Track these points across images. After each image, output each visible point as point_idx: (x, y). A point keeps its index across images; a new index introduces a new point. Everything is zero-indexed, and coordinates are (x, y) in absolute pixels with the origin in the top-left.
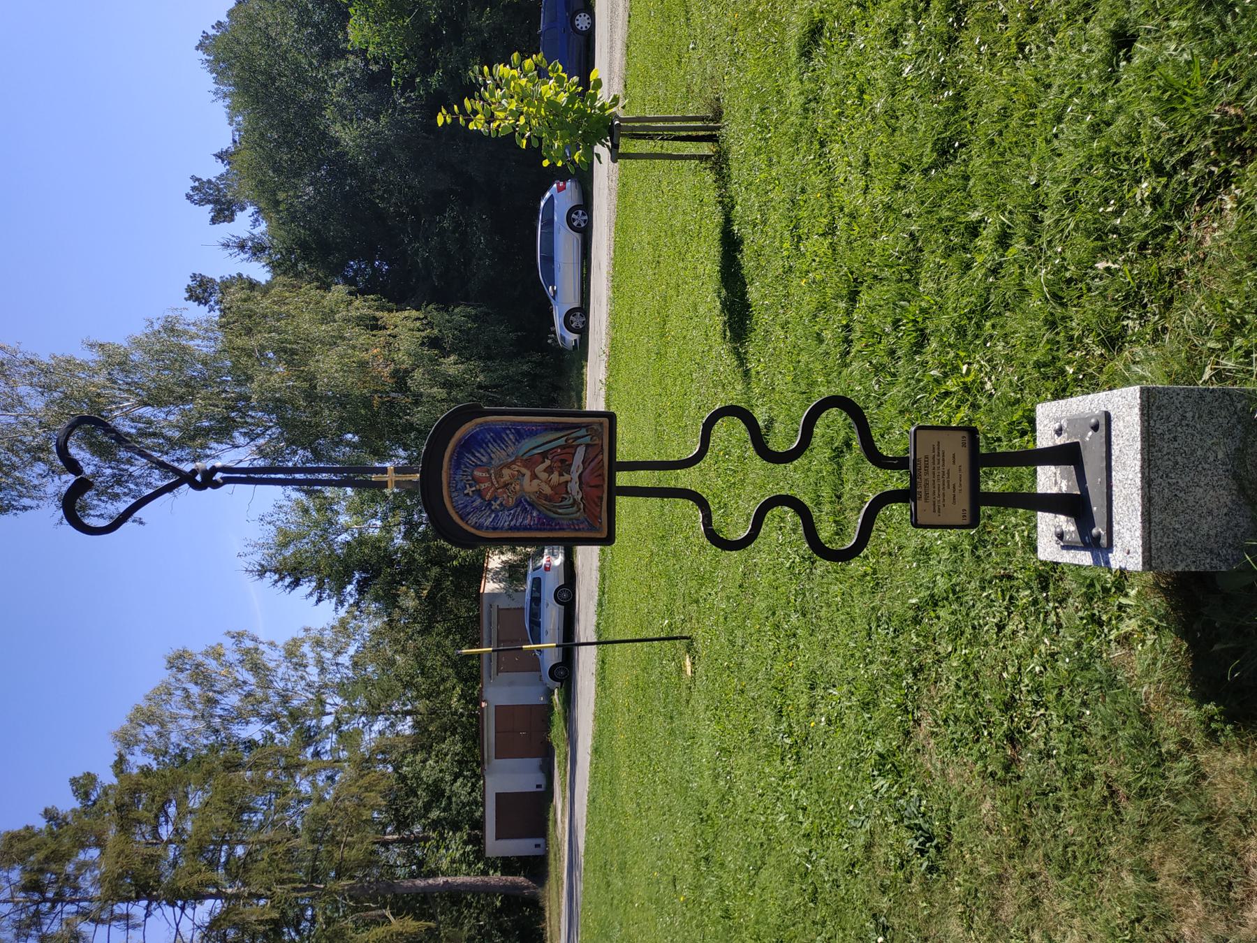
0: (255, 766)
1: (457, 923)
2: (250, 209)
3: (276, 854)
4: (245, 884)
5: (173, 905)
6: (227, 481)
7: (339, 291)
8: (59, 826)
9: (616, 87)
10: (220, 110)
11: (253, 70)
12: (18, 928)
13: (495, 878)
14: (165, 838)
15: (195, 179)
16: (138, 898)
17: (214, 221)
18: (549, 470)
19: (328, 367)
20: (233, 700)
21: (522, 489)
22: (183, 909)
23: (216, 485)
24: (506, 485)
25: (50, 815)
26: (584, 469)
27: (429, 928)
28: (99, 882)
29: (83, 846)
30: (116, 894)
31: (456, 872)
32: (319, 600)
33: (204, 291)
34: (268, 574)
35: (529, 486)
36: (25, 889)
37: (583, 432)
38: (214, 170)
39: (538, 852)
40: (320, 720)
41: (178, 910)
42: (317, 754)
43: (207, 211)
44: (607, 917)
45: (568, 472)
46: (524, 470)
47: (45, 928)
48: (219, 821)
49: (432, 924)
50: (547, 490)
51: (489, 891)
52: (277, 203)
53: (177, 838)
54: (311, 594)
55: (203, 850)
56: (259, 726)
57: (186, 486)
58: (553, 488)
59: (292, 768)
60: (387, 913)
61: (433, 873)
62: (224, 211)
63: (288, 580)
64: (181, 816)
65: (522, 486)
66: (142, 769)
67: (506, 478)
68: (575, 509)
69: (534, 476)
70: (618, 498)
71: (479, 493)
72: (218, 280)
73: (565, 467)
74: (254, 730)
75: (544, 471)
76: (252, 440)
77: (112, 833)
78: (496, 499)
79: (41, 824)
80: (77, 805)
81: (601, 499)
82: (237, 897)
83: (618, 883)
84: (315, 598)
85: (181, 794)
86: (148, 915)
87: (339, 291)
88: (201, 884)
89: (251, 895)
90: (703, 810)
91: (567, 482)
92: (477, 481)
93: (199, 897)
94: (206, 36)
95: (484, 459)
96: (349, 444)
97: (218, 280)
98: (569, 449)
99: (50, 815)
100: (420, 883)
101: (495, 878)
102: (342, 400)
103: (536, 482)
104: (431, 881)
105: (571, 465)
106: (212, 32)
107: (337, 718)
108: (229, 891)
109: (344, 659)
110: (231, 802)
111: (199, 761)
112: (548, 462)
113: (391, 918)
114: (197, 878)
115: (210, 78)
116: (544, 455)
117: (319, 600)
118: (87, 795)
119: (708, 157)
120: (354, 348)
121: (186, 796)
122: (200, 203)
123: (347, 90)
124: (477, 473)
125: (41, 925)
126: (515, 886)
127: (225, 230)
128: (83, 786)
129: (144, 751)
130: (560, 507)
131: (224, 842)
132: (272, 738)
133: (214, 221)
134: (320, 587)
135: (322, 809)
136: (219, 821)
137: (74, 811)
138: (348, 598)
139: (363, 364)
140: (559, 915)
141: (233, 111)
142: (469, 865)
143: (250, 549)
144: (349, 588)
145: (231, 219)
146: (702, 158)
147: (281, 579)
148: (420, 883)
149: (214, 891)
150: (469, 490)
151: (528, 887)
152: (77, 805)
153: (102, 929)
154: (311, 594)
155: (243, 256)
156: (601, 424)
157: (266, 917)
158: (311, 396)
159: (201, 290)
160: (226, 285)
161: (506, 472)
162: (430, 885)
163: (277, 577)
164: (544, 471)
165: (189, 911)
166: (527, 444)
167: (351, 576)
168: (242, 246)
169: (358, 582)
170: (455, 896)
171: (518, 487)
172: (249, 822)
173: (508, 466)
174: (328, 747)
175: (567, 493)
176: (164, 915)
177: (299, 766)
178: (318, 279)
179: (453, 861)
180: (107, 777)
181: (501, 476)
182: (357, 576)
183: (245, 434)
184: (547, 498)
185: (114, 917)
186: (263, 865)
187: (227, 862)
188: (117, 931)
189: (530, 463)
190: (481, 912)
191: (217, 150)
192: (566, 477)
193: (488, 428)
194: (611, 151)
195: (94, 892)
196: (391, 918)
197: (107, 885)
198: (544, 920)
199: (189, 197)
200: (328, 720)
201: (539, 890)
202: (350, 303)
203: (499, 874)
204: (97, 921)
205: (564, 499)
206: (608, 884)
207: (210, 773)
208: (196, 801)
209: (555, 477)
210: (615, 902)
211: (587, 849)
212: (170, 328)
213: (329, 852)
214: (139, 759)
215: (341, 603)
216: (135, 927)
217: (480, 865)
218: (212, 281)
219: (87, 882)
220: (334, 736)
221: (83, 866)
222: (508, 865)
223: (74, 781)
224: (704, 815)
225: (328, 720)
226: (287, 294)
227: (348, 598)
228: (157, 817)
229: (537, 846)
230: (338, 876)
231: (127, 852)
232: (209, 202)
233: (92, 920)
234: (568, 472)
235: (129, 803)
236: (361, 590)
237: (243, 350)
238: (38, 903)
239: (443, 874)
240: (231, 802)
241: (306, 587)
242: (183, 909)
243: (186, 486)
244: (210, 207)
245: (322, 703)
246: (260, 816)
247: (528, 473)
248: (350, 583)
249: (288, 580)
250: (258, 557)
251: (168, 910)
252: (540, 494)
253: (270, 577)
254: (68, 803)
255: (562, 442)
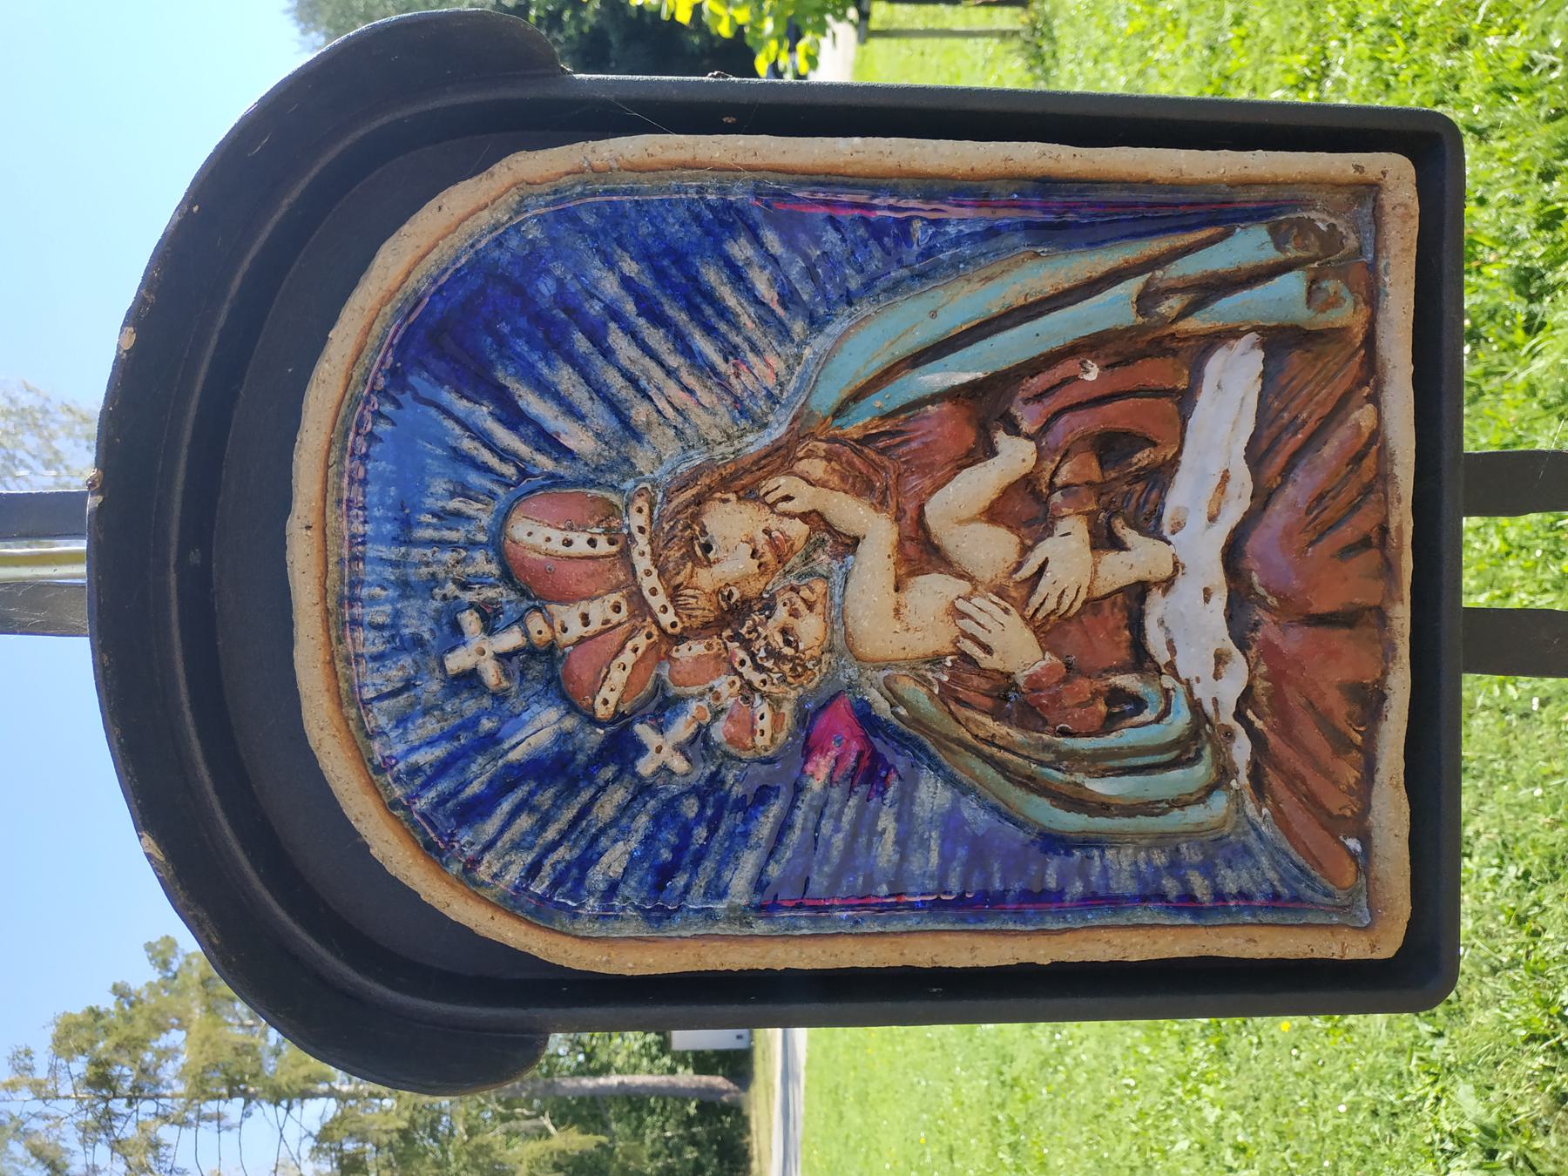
1: (637, 1134)
5: (277, 1104)
9: (751, 310)
12: (85, 1131)
13: (686, 1078)
16: (231, 1095)
18: (1024, 509)
21: (841, 643)
24: (733, 614)
25: (120, 991)
26: (1263, 498)
27: (600, 1145)
28: (180, 1076)
29: (162, 1029)
31: (635, 1069)
35: (892, 621)
36: (89, 1083)
37: (1248, 246)
39: (741, 1045)
41: (281, 1111)
44: (839, 1160)
45: (1150, 524)
46: (850, 512)
47: (117, 1132)
49: (604, 1139)
50: (1016, 650)
51: (682, 1096)
58: (1047, 630)
60: (546, 1121)
61: (605, 1069)
65: (837, 618)
67: (733, 566)
68: (1201, 772)
69: (922, 552)
70: (1468, 680)
71: (543, 667)
73: (1127, 482)
75: (994, 514)
77: (197, 1012)
78: (663, 706)
79: (108, 1003)
80: (155, 976)
81: (1370, 701)
82: (354, 1096)
83: (854, 1117)
86: (247, 1115)
88: (308, 1079)
90: (1005, 1068)
91: (1139, 592)
92: (530, 586)
95: (578, 439)
98: (1157, 362)
99: (120, 991)
100: (588, 1083)
101: (686, 1078)
103: (933, 590)
104: (602, 1081)
105: (1162, 475)
112: (1016, 454)
113: (552, 1129)
116: (987, 407)
118: (165, 965)
119: (1015, 33)
124: (537, 535)
125: (111, 1128)
126: (711, 1090)
130: (1101, 764)
137: (150, 985)
140: (770, 1130)
142: (652, 1060)
146: (1004, 35)
148: (588, 1083)
150: (478, 652)
151: (728, 1091)
152: (155, 976)
153: (187, 1134)
156: (1368, 191)
161: (732, 525)
162: (602, 1087)
164: (994, 514)
165: (296, 1111)
166: (869, 339)
170: (635, 1102)
171: (810, 629)
173: (743, 482)
175: (1140, 659)
176: (265, 1113)
179: (631, 1054)
181: (701, 551)
184: (1006, 696)
185: (201, 1117)
188: (207, 1131)
189: (886, 457)
190: (667, 1119)
192: (1141, 557)
193: (607, 220)
194: (857, 26)
195: (180, 1088)
196: (552, 1129)
197: (190, 1080)
198: (749, 1132)
201: (743, 1095)
203: (690, 1071)
204: (184, 1124)
205: (1123, 706)
206: (841, 1116)
209: (1068, 561)
210: (852, 1143)
211: (809, 1061)
216: (229, 1128)
217: (667, 1060)
219: (168, 1071)
221: (167, 1053)
222: (703, 1062)
223: (149, 947)
224: (1008, 1078)
229: (739, 1037)
231: (214, 1040)
234: (1150, 524)
238: (106, 1100)
239: (618, 1071)
242: (288, 1109)
247: (878, 532)
251: (269, 1109)
252: (962, 676)
254: (108, 1003)
255: (1113, 309)
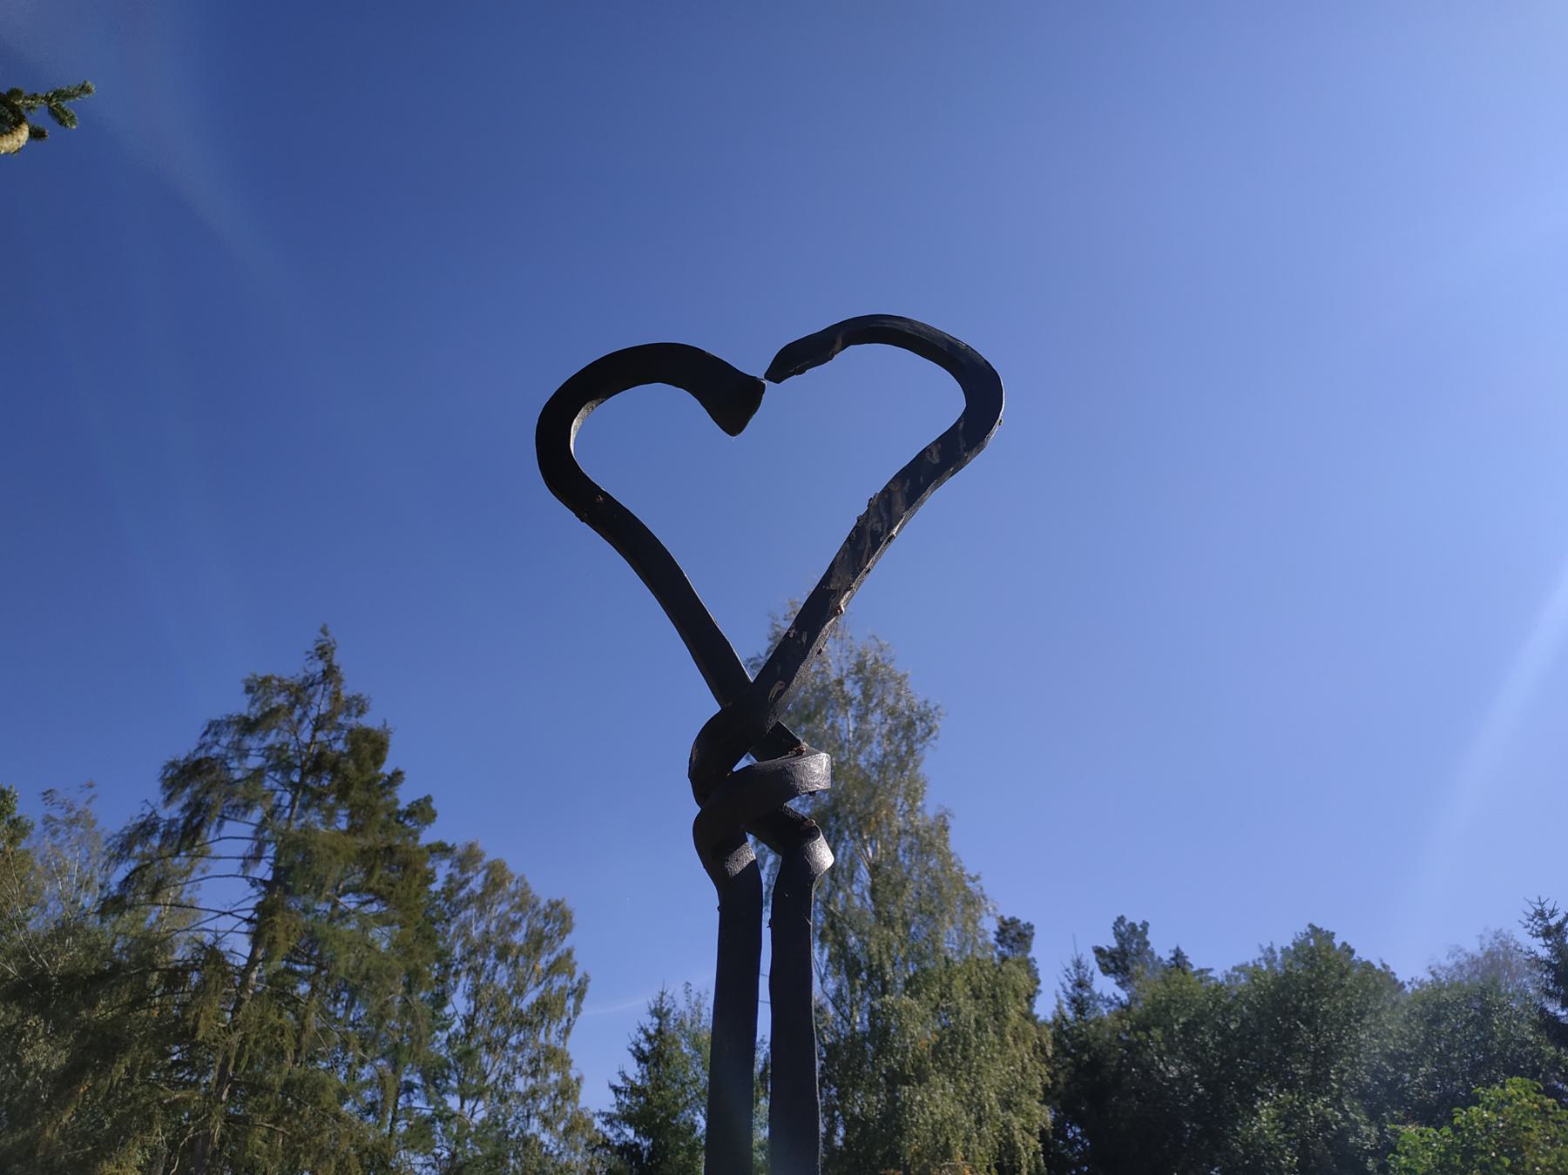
0: (407, 1009)
2: (1123, 996)
3: (282, 1034)
4: (257, 995)
5: (256, 910)
6: (737, 902)
7: (1045, 1116)
8: (381, 787)
10: (1250, 955)
11: (1313, 994)
14: (341, 900)
15: (1145, 925)
17: (1099, 951)
19: (937, 1102)
20: (502, 976)
22: (249, 921)
23: (713, 843)
25: (396, 777)
30: (289, 844)
32: (616, 1090)
33: (1014, 939)
34: (656, 1021)
38: (1161, 947)
40: (454, 1092)
41: (247, 915)
42: (409, 1087)
43: (1110, 942)
48: (346, 962)
52: (1146, 1029)
53: (336, 914)
54: (625, 1078)
55: (312, 947)
56: (462, 1011)
57: (711, 707)
59: (395, 1055)
62: (1117, 961)
63: (646, 1047)
64: (363, 919)
66: (432, 871)
72: (1030, 956)
74: (459, 1004)
76: (834, 1002)
84: (620, 1083)
85: (392, 917)
87: (1045, 1116)
88: (273, 940)
89: (240, 1001)
93: (256, 939)
94: (1331, 936)
96: (831, 1131)
97: (1030, 956)
102: (894, 1120)
106: (1338, 942)
107: (454, 1115)
108: (254, 975)
109: (535, 1125)
110: (367, 977)
111: (430, 939)
114: (281, 936)
115: (1288, 943)
117: (616, 1090)
120: (968, 1139)
121: (390, 923)
122: (1118, 935)
123: (1326, 1126)
127: (1092, 963)
128: (422, 811)
129: (450, 878)
131: (320, 967)
132: (443, 1028)
133: (1099, 951)
134: (635, 1091)
135: (329, 1097)
136: (346, 962)
137: (396, 802)
138: (616, 1131)
139: (946, 1152)
141: (1253, 973)
143: (694, 998)
144: (630, 1132)
145: (1106, 971)
147: (649, 1038)
149: (260, 955)
152: (402, 806)
154: (625, 1078)
155: (1069, 985)
157: (202, 1022)
158: (896, 1079)
159: (1015, 935)
160: (1029, 966)
163: (652, 1032)
165: (245, 927)
167: (647, 1135)
168: (1081, 984)
169: (637, 1145)
172: (336, 999)
174: (417, 1103)
177: (396, 1066)
178: (1055, 1083)
180: (428, 836)
182: (646, 1144)
183: (839, 990)
186: (273, 1018)
187: (294, 973)
191: (1185, 951)
197: (301, 836)
199: (1121, 920)
200: (453, 1102)
202: (1029, 1131)
207: (408, 953)
208: (382, 938)
212: (971, 901)
213: (268, 1106)
214: (442, 870)
215: (610, 1120)
218: (1028, 948)
219: (314, 817)
220: (429, 1113)
225: (453, 1102)
226: (1030, 1044)
227: (616, 1131)
228: (370, 890)
230: (230, 1120)
232: (1121, 945)
233: (264, 821)
235: (392, 856)
236: (628, 1150)
237: (949, 986)
240: (367, 977)
241: (634, 1070)
242: (249, 921)
243: (711, 707)
244: (1114, 944)
245: (479, 1095)
246: (340, 1014)
248: (636, 1133)
249: (646, 1047)
250: (682, 1005)
251: (252, 903)
253: (652, 1024)
254: (405, 796)
